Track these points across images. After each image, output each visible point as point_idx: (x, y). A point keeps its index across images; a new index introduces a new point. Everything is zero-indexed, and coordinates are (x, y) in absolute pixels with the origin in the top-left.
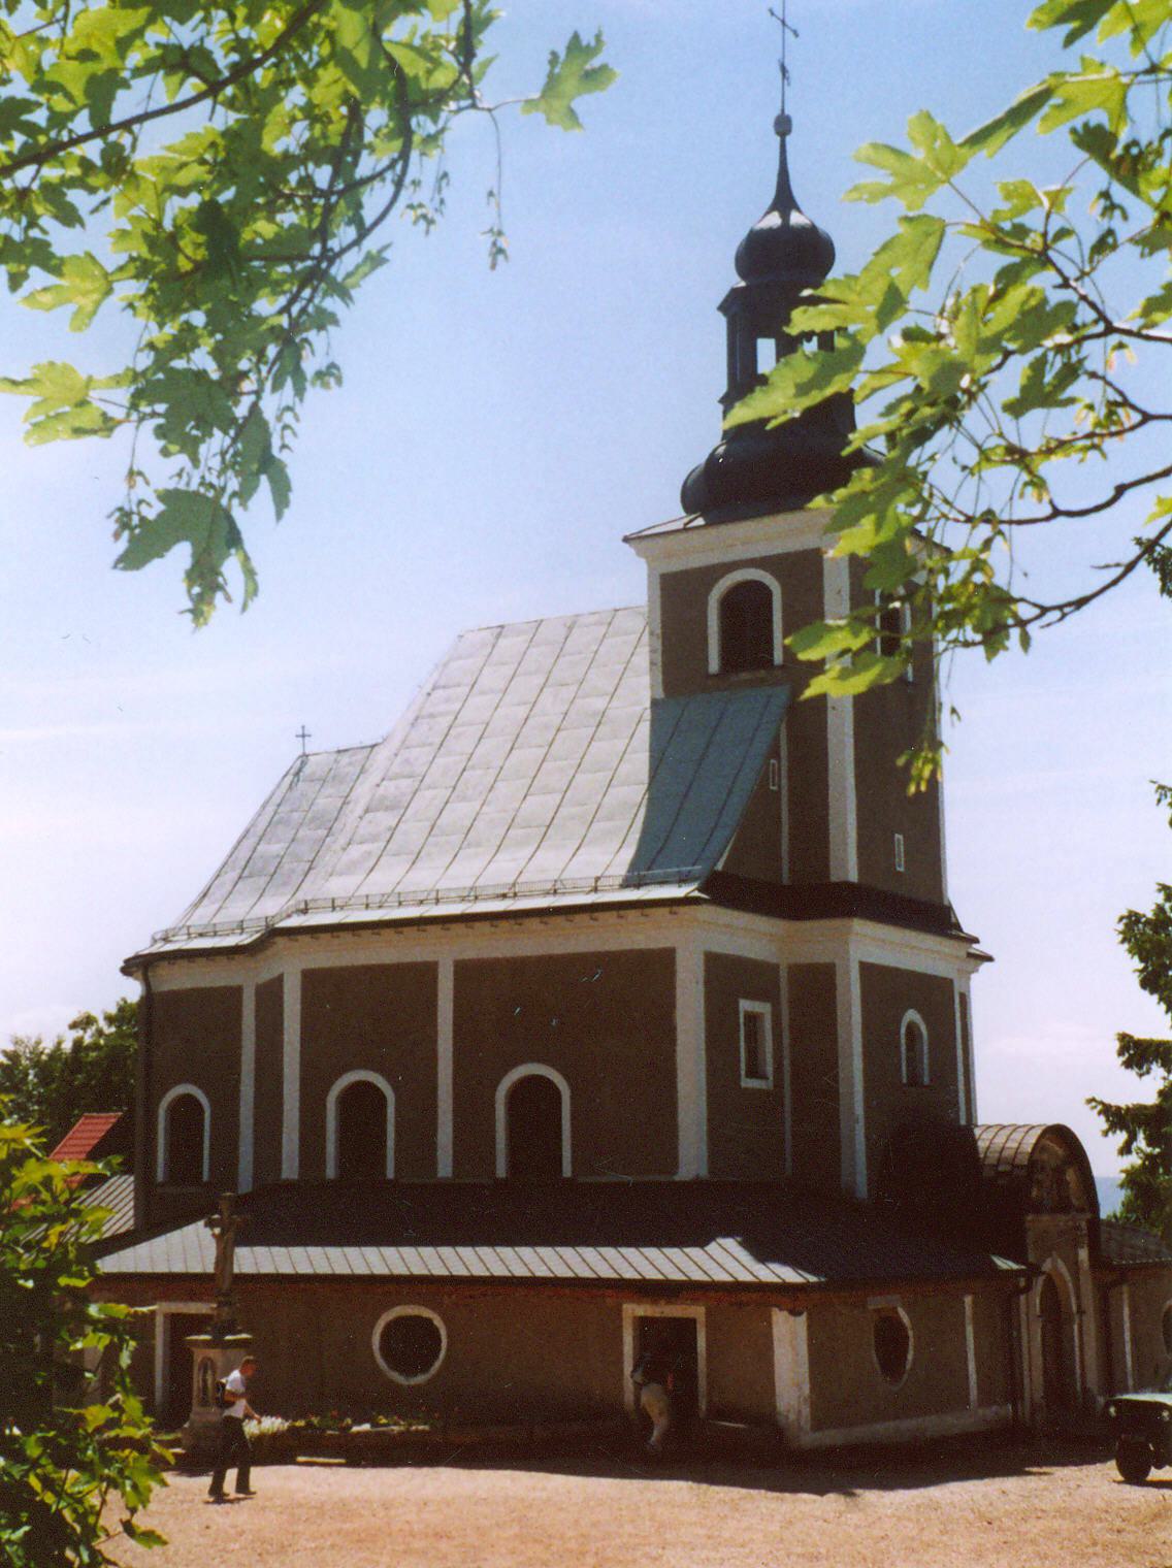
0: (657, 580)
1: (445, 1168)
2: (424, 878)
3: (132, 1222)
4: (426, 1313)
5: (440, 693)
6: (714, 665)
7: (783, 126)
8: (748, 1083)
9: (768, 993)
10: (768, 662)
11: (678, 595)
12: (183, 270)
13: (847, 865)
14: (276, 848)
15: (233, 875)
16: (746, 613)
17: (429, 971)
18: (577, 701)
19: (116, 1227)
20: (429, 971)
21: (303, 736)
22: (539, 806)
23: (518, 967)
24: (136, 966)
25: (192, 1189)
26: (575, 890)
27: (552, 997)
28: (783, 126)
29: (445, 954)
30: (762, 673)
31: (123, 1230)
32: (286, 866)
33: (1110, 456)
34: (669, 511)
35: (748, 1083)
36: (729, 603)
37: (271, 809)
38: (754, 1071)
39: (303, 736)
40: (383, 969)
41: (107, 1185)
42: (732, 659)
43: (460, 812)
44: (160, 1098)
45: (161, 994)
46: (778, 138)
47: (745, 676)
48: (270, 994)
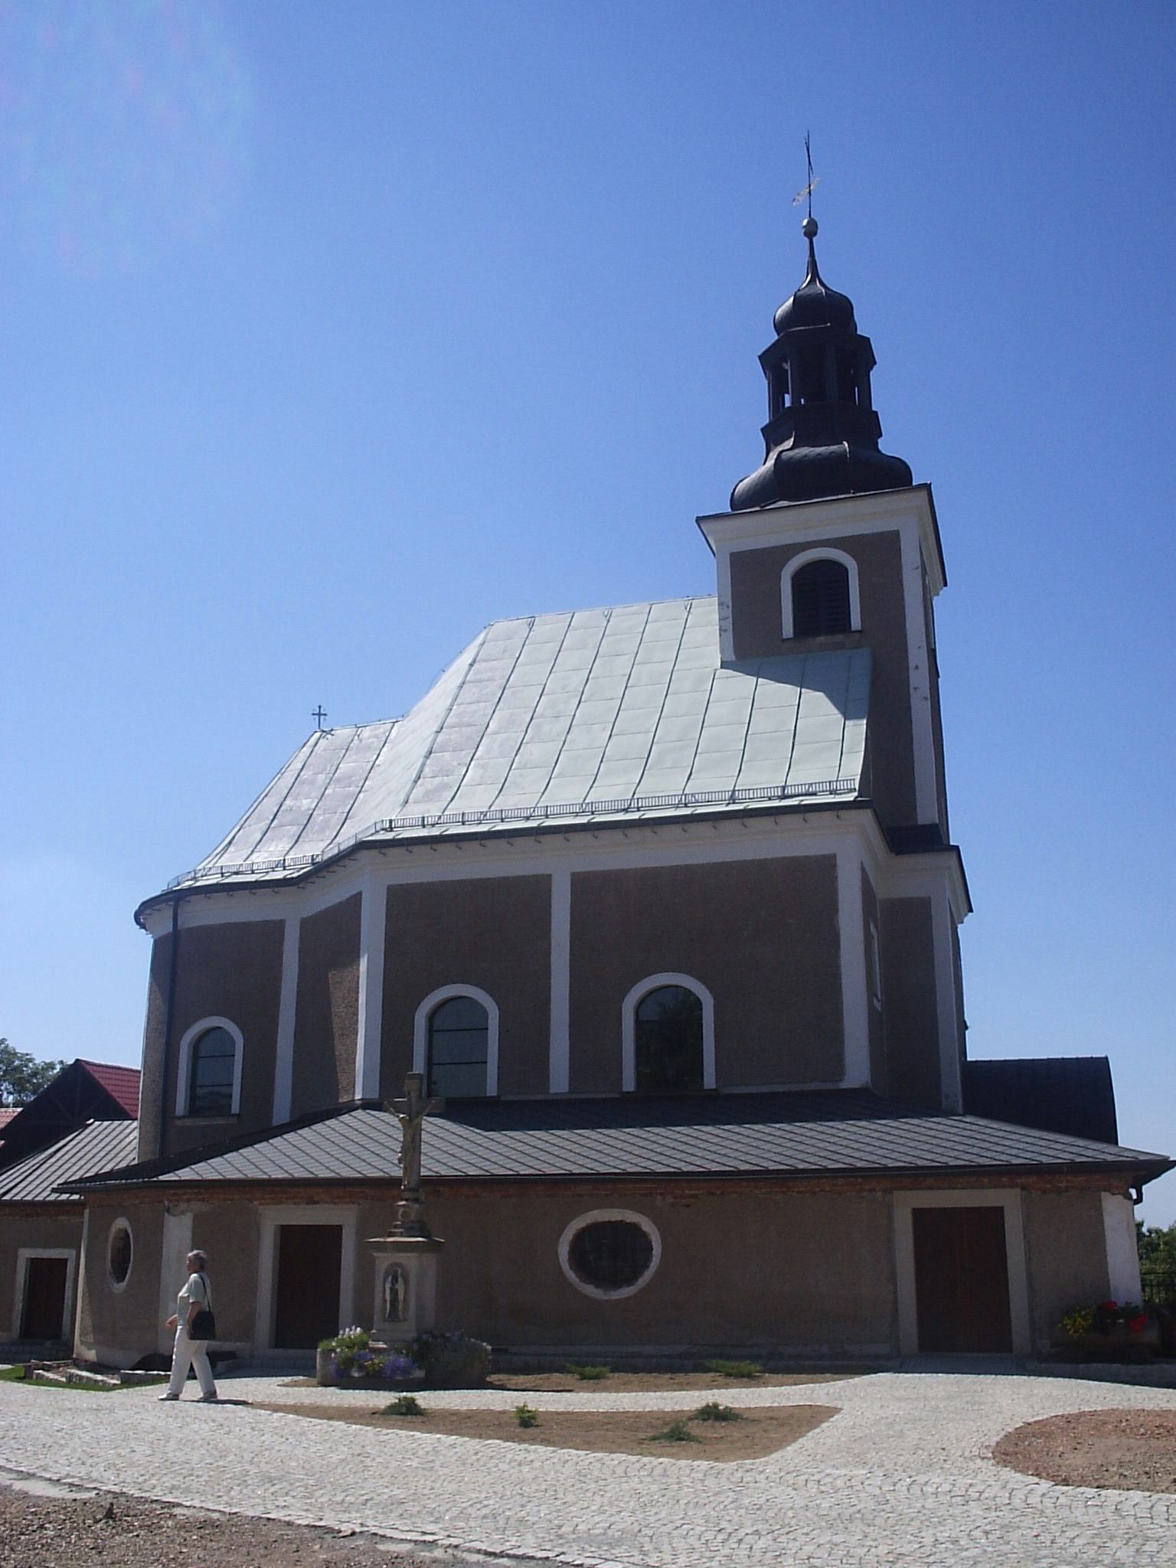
3: (134, 1154)
4: (631, 1217)
6: (788, 630)
14: (306, 804)
16: (821, 594)
17: (541, 885)
19: (118, 1159)
20: (541, 885)
21: (320, 714)
23: (651, 878)
24: (144, 914)
25: (220, 1121)
28: (811, 231)
29: (561, 868)
30: (839, 638)
31: (123, 1165)
32: (319, 818)
36: (800, 579)
39: (320, 714)
40: (484, 883)
41: (87, 1131)
42: (806, 626)
44: (188, 1026)
45: (190, 930)
46: (807, 240)
47: (822, 639)
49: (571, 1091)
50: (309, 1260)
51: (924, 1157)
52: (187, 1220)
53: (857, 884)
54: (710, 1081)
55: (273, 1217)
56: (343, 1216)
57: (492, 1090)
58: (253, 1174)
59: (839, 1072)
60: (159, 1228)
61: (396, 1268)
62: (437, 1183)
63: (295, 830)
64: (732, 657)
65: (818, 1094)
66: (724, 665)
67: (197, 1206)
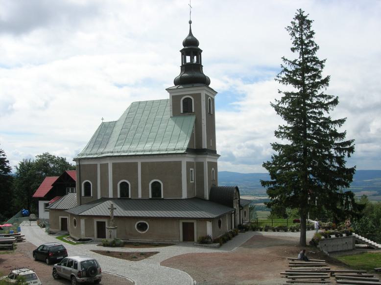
0: (232, 184)
1: (140, 196)
2: (133, 147)
5: (130, 113)
6: (182, 112)
7: (190, 22)
8: (191, 182)
9: (193, 167)
10: (192, 112)
11: (175, 99)
12: (203, 147)
13: (83, 222)
14: (100, 140)
15: (92, 144)
16: (187, 103)
18: (145, 112)
22: (153, 134)
26: (154, 151)
27: (160, 168)
28: (190, 22)
32: (103, 143)
33: (289, 19)
34: (172, 85)
35: (191, 182)
37: (98, 132)
38: (192, 181)
42: (185, 111)
43: (138, 135)
48: (104, 167)
49: (187, 197)
50: (101, 228)
51: (301, 279)
52: (84, 220)
53: (158, 251)
54: (162, 197)
55: (95, 221)
56: (106, 220)
57: (140, 196)
58: (86, 214)
59: (181, 196)
60: (80, 221)
61: (111, 232)
62: (115, 217)
63: (99, 145)
64: (172, 116)
65: (179, 199)
66: (171, 117)
67: (85, 218)
